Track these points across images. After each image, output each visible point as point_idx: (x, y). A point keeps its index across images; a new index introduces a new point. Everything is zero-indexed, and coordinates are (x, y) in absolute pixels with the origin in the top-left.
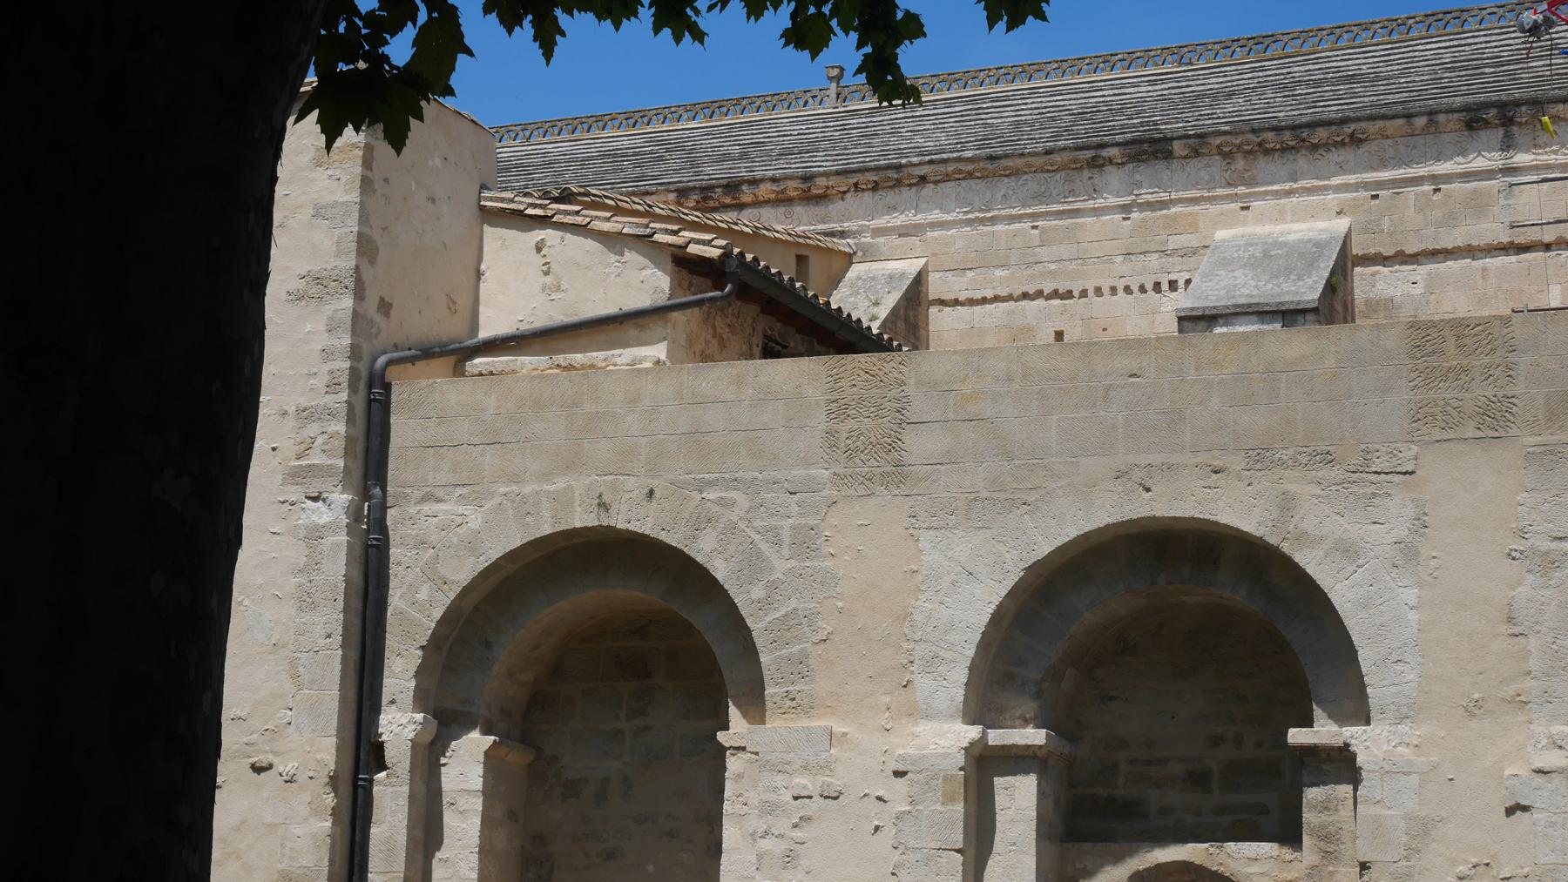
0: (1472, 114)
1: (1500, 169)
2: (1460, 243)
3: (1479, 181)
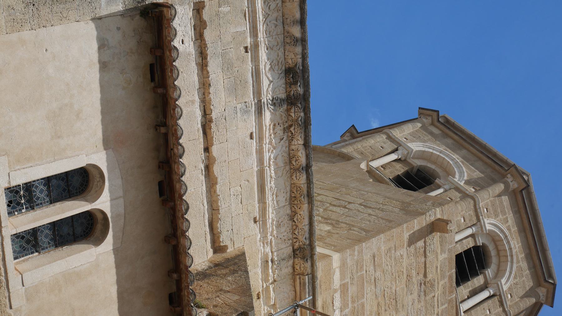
0: (300, 75)
1: (261, 101)
2: (212, 76)
3: (253, 84)
